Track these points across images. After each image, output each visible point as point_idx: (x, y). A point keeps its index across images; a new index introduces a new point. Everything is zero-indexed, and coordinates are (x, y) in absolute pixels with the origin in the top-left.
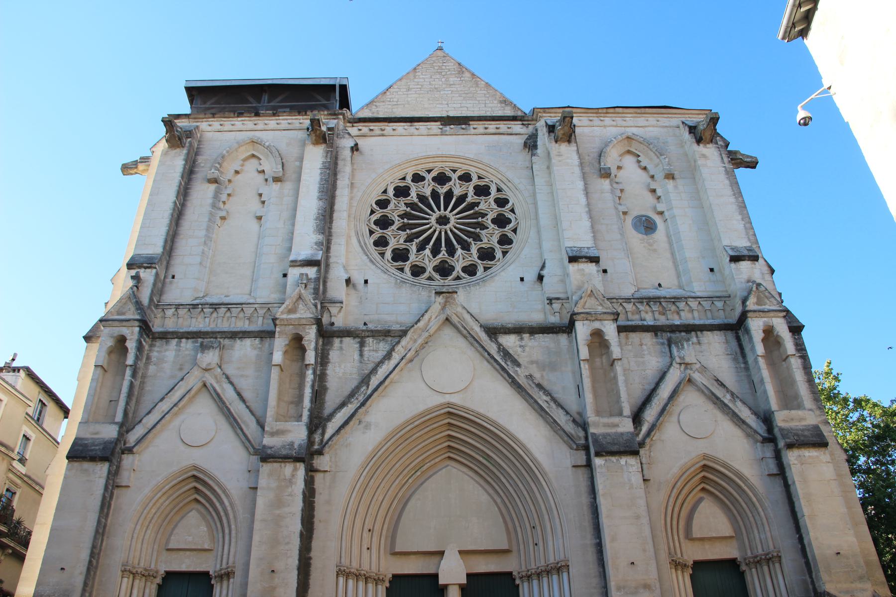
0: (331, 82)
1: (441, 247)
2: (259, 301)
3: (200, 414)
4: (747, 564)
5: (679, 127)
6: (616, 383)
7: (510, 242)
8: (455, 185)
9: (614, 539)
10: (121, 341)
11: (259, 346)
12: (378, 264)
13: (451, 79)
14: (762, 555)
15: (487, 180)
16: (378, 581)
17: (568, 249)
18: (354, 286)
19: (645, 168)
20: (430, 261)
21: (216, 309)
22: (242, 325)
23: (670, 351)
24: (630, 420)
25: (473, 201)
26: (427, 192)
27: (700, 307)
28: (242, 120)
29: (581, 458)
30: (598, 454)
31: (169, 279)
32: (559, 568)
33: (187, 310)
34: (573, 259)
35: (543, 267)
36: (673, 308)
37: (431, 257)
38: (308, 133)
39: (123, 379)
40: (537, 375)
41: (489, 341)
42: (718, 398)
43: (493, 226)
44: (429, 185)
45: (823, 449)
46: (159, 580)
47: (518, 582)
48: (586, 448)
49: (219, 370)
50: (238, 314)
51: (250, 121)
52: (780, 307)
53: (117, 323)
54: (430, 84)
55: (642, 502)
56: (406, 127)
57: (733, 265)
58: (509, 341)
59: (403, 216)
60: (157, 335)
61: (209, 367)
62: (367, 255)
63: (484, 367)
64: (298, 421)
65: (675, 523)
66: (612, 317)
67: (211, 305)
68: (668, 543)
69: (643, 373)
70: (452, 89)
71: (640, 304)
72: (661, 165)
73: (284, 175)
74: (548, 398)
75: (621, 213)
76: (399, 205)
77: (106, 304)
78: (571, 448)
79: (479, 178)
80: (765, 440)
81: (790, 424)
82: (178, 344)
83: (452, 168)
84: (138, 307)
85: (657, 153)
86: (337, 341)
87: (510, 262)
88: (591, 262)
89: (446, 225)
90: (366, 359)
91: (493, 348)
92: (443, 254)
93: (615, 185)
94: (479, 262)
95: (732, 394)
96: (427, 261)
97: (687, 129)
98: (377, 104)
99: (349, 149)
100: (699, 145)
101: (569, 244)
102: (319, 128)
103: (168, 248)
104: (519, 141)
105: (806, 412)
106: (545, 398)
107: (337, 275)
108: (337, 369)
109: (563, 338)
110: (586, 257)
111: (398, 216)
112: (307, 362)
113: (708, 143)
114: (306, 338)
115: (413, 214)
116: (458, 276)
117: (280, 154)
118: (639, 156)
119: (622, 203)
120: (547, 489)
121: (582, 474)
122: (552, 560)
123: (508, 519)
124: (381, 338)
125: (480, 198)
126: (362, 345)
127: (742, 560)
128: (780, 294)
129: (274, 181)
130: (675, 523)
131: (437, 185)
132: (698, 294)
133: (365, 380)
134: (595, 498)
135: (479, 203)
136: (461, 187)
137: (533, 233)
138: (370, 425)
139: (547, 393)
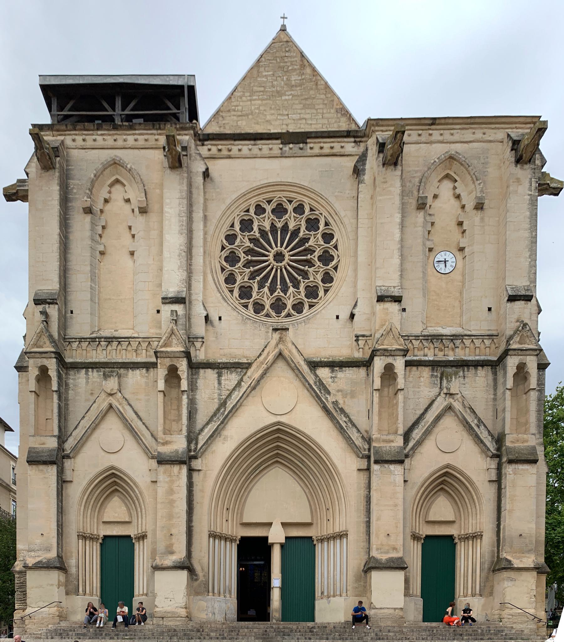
0: (180, 82)
1: (277, 285)
2: (142, 335)
3: (111, 429)
4: (459, 539)
5: (502, 142)
6: (397, 409)
7: (331, 280)
8: (290, 218)
9: (378, 519)
10: (44, 370)
11: (146, 375)
12: (229, 302)
13: (293, 78)
14: (471, 533)
15: (317, 212)
16: (232, 540)
17: (378, 288)
18: (212, 323)
19: (458, 197)
20: (268, 299)
21: (109, 342)
22: (132, 358)
23: (441, 383)
24: (402, 438)
25: (305, 236)
26: (267, 226)
27: (472, 345)
28: (102, 135)
29: (363, 464)
30: (376, 462)
31: (69, 315)
32: (342, 536)
33: (88, 343)
34: (381, 299)
35: (355, 305)
36: (451, 345)
37: (269, 295)
38: (165, 154)
39: (53, 402)
40: (341, 402)
41: (310, 373)
42: (467, 423)
43: (318, 263)
44: (269, 218)
45: (533, 465)
46: (100, 541)
47: (315, 542)
48: (368, 457)
49: (120, 395)
50: (127, 347)
51: (109, 135)
52: (537, 346)
53: (38, 355)
54: (273, 86)
55: (401, 496)
56: (250, 147)
57: (509, 304)
58: (324, 373)
59: (248, 253)
60: (69, 366)
61: (112, 393)
62: (220, 293)
63: (305, 394)
64: (179, 434)
65: (418, 510)
66: (402, 353)
67: (105, 338)
68: (412, 523)
69: (417, 401)
70: (293, 92)
71: (425, 341)
72: (474, 192)
73: (147, 205)
74: (346, 420)
75: (427, 249)
76: (244, 241)
77: (24, 337)
78: (358, 457)
79: (311, 210)
80: (494, 456)
81: (516, 445)
82: (87, 373)
83: (288, 199)
84: (51, 340)
85: (474, 176)
86: (202, 371)
87: (330, 300)
88: (395, 301)
89: (281, 263)
90: (223, 387)
91: (311, 379)
92: (278, 292)
93: (428, 218)
94: (306, 300)
95: (479, 420)
96: (265, 299)
97: (510, 144)
98: (224, 114)
99: (201, 175)
100: (516, 166)
101: (379, 283)
102: (174, 148)
103: (62, 283)
104: (349, 163)
105: (530, 436)
106: (344, 419)
107: (199, 312)
108: (203, 396)
109: (362, 371)
110: (392, 297)
111: (244, 252)
112: (183, 389)
113: (526, 163)
114: (180, 369)
115: (256, 251)
116: (289, 314)
117: (141, 180)
118: (456, 181)
119: (430, 238)
120: (339, 485)
121: (363, 476)
122: (338, 531)
123: (312, 504)
124: (233, 369)
125: (311, 233)
126: (220, 375)
127: (457, 536)
128: (539, 333)
129: (140, 212)
130: (418, 510)
131: (275, 218)
132: (473, 333)
133: (223, 404)
134: (370, 492)
135: (309, 239)
136: (295, 220)
137: (350, 273)
138: (227, 437)
139: (347, 416)
